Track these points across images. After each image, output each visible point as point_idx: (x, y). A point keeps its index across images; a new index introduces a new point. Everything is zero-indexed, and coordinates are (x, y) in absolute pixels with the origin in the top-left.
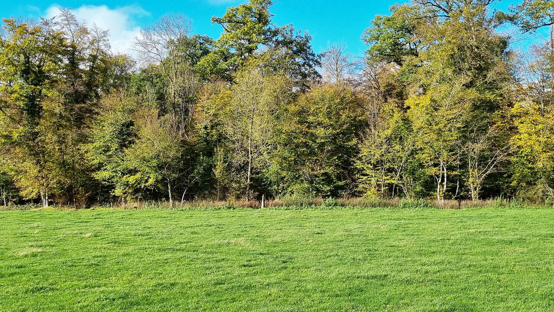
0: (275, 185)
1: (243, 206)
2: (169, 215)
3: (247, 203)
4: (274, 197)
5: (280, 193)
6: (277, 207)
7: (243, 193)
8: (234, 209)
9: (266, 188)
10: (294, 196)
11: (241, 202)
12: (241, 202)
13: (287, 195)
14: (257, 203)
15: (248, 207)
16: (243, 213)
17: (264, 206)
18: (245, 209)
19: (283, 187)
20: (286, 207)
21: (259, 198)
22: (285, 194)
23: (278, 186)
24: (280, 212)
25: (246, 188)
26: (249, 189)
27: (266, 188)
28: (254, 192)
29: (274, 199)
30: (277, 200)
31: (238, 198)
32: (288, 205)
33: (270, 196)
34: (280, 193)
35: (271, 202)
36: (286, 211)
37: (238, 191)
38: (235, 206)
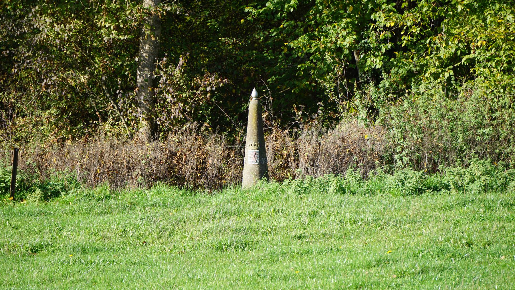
0: (336, 17)
1: (117, 175)
2: (421, 110)
3: (142, 148)
4: (331, 107)
5: (376, 76)
6: (350, 177)
7: (118, 84)
8: (50, 194)
9: (277, 46)
10: (475, 93)
11: (100, 145)
12: (101, 142)
13: (428, 92)
14: (214, 150)
15: (152, 179)
16: (110, 223)
17: (263, 172)
18: (130, 193)
19: (396, 33)
20: (414, 177)
21: (223, 118)
22: (410, 78)
23: (361, 27)
24: (370, 208)
25: (132, 48)
26: (158, 53)
27: (277, 46)
28: (191, 71)
29: (332, 120)
30: (353, 126)
31: (80, 117)
32: (430, 160)
33: (299, 100)
34: (376, 76)
35: (308, 140)
36: (416, 201)
37: (83, 65)
38: (56, 178)
